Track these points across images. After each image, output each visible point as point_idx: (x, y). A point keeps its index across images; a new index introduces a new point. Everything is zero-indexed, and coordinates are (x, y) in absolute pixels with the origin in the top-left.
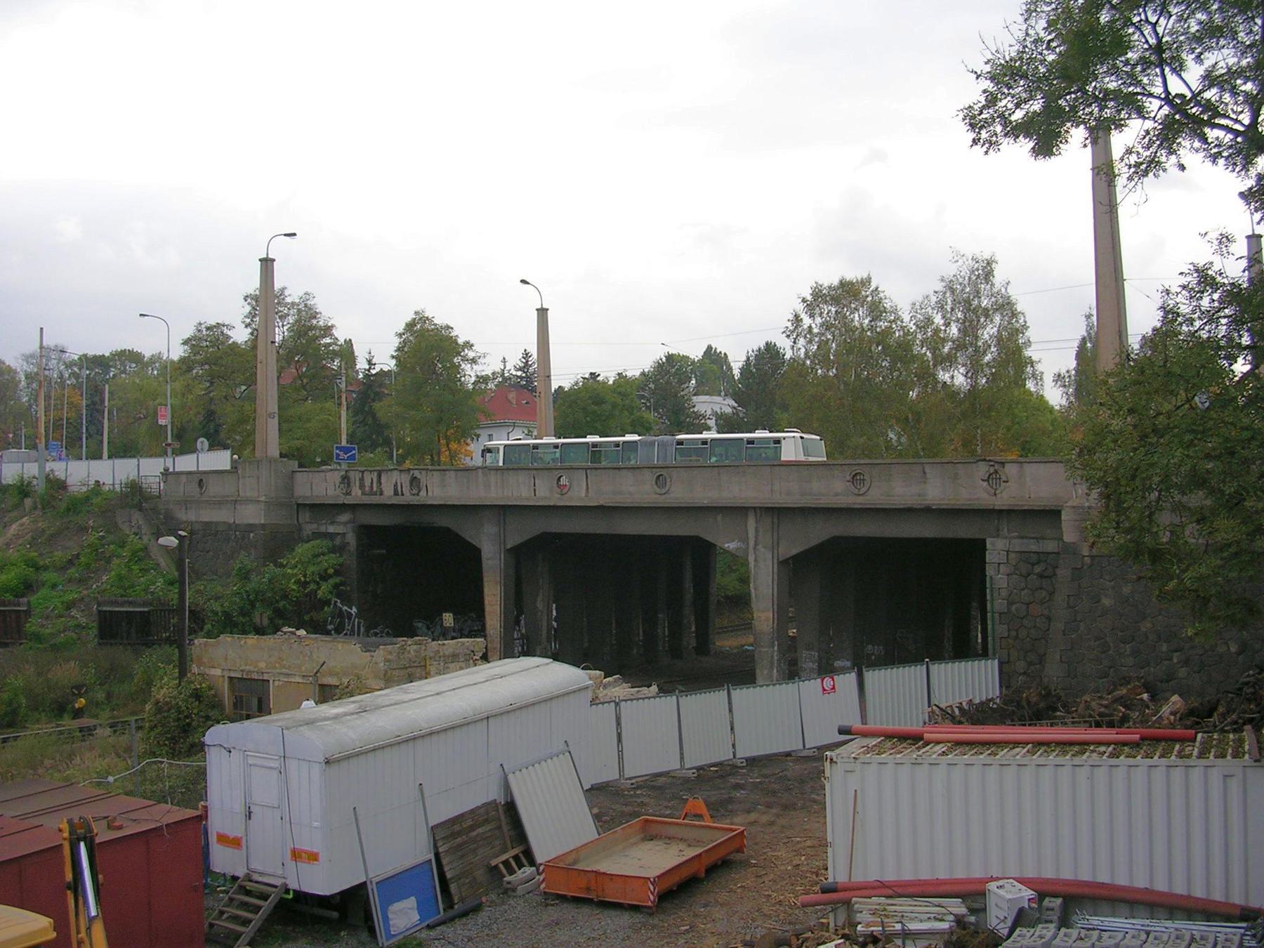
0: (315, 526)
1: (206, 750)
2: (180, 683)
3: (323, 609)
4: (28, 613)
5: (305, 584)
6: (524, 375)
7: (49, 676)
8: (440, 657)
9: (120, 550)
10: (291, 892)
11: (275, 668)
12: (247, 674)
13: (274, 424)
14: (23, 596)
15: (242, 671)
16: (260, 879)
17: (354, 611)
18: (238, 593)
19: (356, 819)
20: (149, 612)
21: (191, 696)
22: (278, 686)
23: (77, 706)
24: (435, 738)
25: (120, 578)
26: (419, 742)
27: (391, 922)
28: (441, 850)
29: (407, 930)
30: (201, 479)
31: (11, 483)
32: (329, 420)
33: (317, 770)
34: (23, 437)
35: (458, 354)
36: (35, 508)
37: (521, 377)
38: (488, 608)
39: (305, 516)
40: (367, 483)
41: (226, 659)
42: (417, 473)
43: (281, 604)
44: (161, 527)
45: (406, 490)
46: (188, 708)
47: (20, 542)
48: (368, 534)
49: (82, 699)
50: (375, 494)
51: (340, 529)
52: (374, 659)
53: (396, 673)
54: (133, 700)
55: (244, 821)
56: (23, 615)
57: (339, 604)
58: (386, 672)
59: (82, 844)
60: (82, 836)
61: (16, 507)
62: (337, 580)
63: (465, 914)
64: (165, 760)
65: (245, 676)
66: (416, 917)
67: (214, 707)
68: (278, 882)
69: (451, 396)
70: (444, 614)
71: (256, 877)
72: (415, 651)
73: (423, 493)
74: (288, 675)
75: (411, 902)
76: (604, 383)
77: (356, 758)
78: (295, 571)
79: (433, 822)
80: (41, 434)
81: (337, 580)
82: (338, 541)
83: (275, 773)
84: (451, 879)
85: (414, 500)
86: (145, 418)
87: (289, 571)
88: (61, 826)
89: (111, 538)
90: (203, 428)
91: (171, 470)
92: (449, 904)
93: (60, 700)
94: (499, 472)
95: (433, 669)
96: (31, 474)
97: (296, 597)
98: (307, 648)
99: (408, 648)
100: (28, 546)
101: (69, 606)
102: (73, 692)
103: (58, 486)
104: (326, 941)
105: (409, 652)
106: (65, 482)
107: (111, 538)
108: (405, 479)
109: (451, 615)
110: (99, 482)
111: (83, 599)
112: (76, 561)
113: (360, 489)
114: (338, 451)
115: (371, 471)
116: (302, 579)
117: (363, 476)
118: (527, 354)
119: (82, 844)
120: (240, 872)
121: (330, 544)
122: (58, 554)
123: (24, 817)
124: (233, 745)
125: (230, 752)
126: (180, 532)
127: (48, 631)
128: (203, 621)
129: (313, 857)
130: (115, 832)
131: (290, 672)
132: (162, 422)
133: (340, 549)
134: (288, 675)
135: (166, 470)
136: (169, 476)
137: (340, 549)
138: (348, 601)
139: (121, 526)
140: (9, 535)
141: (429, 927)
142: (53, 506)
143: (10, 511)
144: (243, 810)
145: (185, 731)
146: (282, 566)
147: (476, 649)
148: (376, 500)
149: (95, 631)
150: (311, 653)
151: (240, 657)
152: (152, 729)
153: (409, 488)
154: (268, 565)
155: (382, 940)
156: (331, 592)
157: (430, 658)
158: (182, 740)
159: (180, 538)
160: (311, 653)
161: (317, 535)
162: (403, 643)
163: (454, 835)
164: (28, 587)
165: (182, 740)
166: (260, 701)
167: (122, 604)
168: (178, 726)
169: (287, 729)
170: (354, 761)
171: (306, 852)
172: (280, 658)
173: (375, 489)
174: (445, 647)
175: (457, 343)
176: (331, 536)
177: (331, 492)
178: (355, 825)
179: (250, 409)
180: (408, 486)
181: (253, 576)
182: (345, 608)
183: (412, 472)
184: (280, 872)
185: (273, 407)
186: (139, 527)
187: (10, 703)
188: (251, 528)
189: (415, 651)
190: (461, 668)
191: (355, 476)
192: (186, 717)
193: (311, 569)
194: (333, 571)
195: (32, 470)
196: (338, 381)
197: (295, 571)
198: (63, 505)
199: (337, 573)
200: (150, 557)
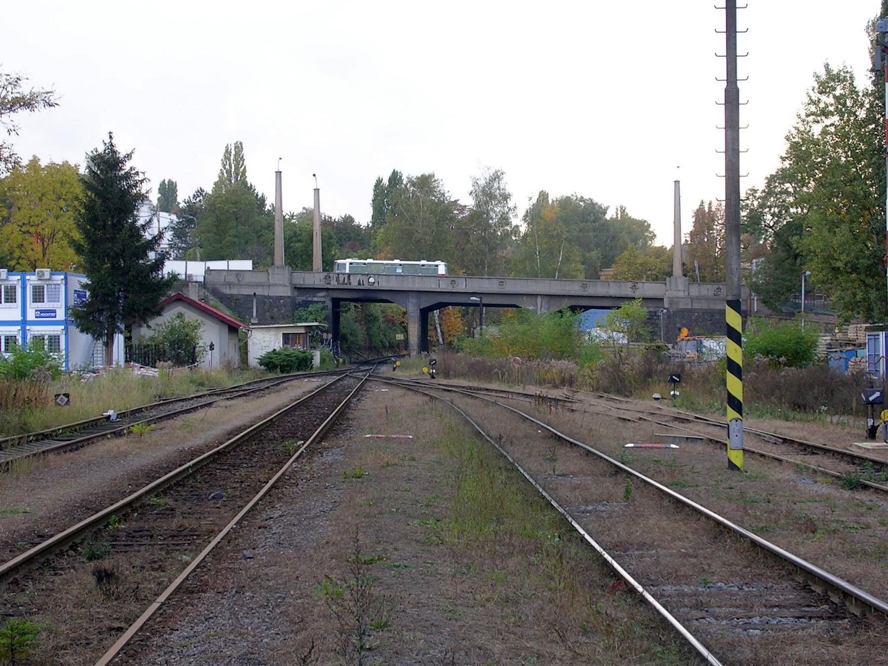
30: (239, 273)
50: (346, 284)
76: (359, 226)
130: (761, 444)
148: (348, 287)
173: (346, 282)
188: (281, 298)
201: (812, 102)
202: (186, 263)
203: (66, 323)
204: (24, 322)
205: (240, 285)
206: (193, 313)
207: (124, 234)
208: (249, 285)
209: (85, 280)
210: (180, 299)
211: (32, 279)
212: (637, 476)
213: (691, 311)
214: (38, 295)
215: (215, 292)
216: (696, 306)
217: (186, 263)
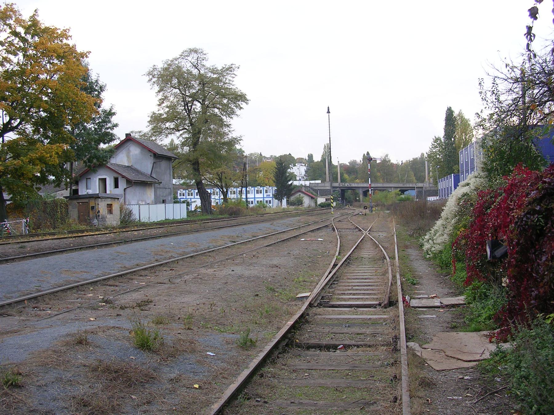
201: (433, 145)
203: (272, 197)
204: (264, 198)
205: (318, 186)
206: (56, 256)
207: (284, 178)
208: (320, 187)
209: (276, 188)
210: (300, 191)
211: (265, 188)
213: (430, 190)
214: (266, 192)
215: (312, 188)
216: (432, 189)
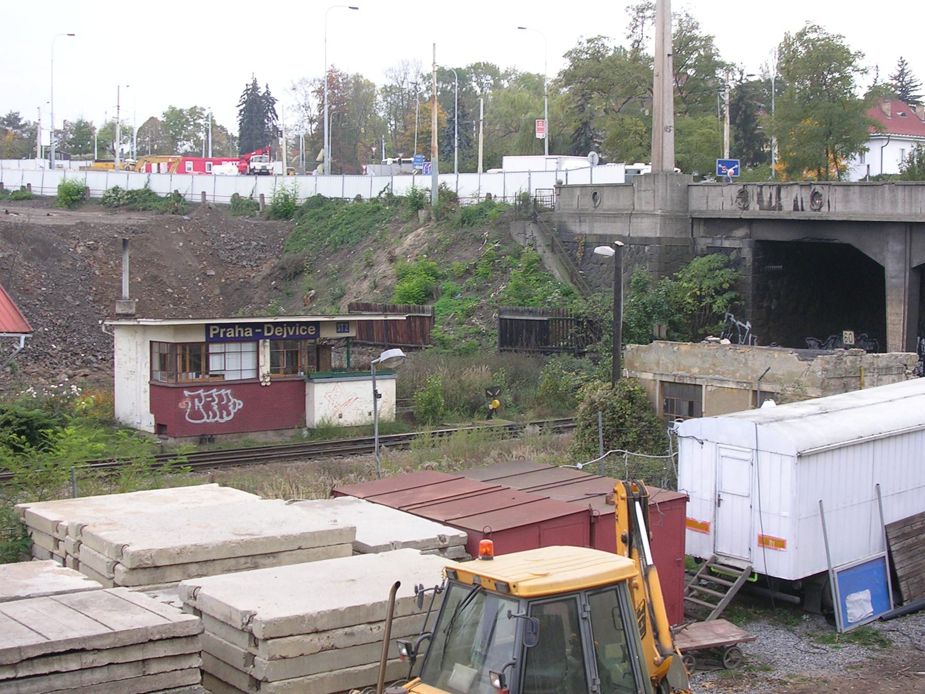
0: (709, 241)
1: (679, 442)
2: (613, 386)
3: (717, 323)
4: (432, 319)
5: (700, 299)
6: (899, 84)
7: (463, 379)
8: (874, 369)
9: (515, 261)
10: (756, 576)
11: (708, 374)
12: (679, 379)
13: (669, 138)
14: (424, 303)
15: (675, 376)
16: (726, 562)
17: (748, 325)
18: (635, 305)
19: (822, 511)
20: (547, 321)
21: (625, 398)
22: (711, 391)
23: (491, 407)
24: (892, 441)
25: (518, 288)
26: (878, 445)
27: (848, 611)
28: (893, 548)
29: (862, 620)
31: (405, 195)
32: (711, 133)
33: (789, 463)
34: (384, 151)
35: (850, 64)
36: (429, 219)
37: (896, 87)
38: (890, 327)
39: (700, 230)
40: (766, 198)
41: (659, 364)
42: (818, 189)
43: (677, 317)
44: (556, 239)
45: (807, 206)
46: (622, 409)
47: (416, 252)
48: (764, 249)
49: (496, 401)
51: (736, 244)
52: (811, 368)
53: (833, 382)
54: (539, 404)
55: (713, 508)
56: (427, 322)
57: (732, 319)
58: (823, 380)
59: (637, 504)
60: (637, 497)
61: (411, 217)
62: (732, 294)
63: (914, 612)
64: (626, 451)
65: (677, 381)
66: (870, 609)
67: (645, 409)
68: (744, 566)
69: (841, 109)
70: (844, 332)
71: (722, 560)
72: (851, 362)
73: (825, 209)
74: (722, 381)
75: (865, 595)
77: (823, 454)
78: (691, 285)
79: (887, 522)
80: (434, 148)
81: (732, 294)
82: (733, 256)
83: (747, 464)
84: (902, 577)
85: (815, 216)
86: (516, 131)
87: (685, 285)
88: (616, 488)
89: (505, 249)
90: (574, 142)
91: (564, 183)
92: (899, 602)
93: (472, 401)
94: (907, 187)
95: (867, 380)
96: (424, 187)
97: (691, 310)
98: (742, 355)
99: (845, 359)
100: (425, 256)
101: (469, 314)
102: (487, 394)
103: (450, 198)
104: (787, 624)
105: (845, 363)
106: (456, 195)
107: (505, 249)
108: (806, 194)
109: (852, 333)
110: (490, 194)
111: (482, 307)
112: (473, 271)
113: (758, 203)
114: (720, 166)
115: (770, 186)
116: (698, 293)
117: (761, 191)
118: (903, 62)
119: (637, 504)
120: (707, 555)
121: (726, 259)
122: (456, 264)
123: (530, 490)
124: (706, 438)
125: (702, 443)
126: (617, 242)
127: (452, 337)
128: (600, 331)
129: (780, 544)
131: (725, 379)
132: (539, 135)
133: (737, 264)
134: (722, 381)
135: (560, 183)
136: (563, 190)
137: (737, 264)
138: (742, 317)
139: (515, 237)
140: (405, 245)
141: (881, 619)
142: (447, 218)
143: (404, 222)
144: (713, 497)
145: (619, 431)
146: (676, 279)
147: (909, 363)
148: (775, 215)
149: (497, 339)
150: (746, 359)
151: (673, 362)
152: (586, 427)
153: (810, 203)
154: (663, 279)
155: (841, 626)
156: (726, 307)
157: (865, 369)
158: (615, 439)
159: (617, 247)
160: (746, 359)
161: (712, 250)
162: (840, 353)
163: (905, 536)
164: (429, 295)
165: (615, 439)
166: (691, 405)
167: (522, 313)
168: (612, 426)
169: (760, 424)
170: (821, 458)
171: (773, 539)
172: (714, 364)
173: (774, 204)
174: (879, 359)
175: (849, 53)
176: (728, 251)
177: (727, 206)
178: (820, 516)
179: (631, 122)
180: (809, 200)
181: (650, 289)
182: (739, 323)
183: (813, 187)
184: (746, 556)
185: (669, 120)
186: (533, 239)
187: (430, 402)
188: (646, 241)
189: (851, 362)
190: (894, 381)
191: (753, 190)
192: (620, 417)
193: (706, 283)
194: (728, 285)
195: (424, 182)
196: (722, 93)
197: (691, 285)
198: (457, 217)
199: (732, 288)
200: (545, 268)
202: (591, 181)
212: (722, 579)
217: (591, 181)
